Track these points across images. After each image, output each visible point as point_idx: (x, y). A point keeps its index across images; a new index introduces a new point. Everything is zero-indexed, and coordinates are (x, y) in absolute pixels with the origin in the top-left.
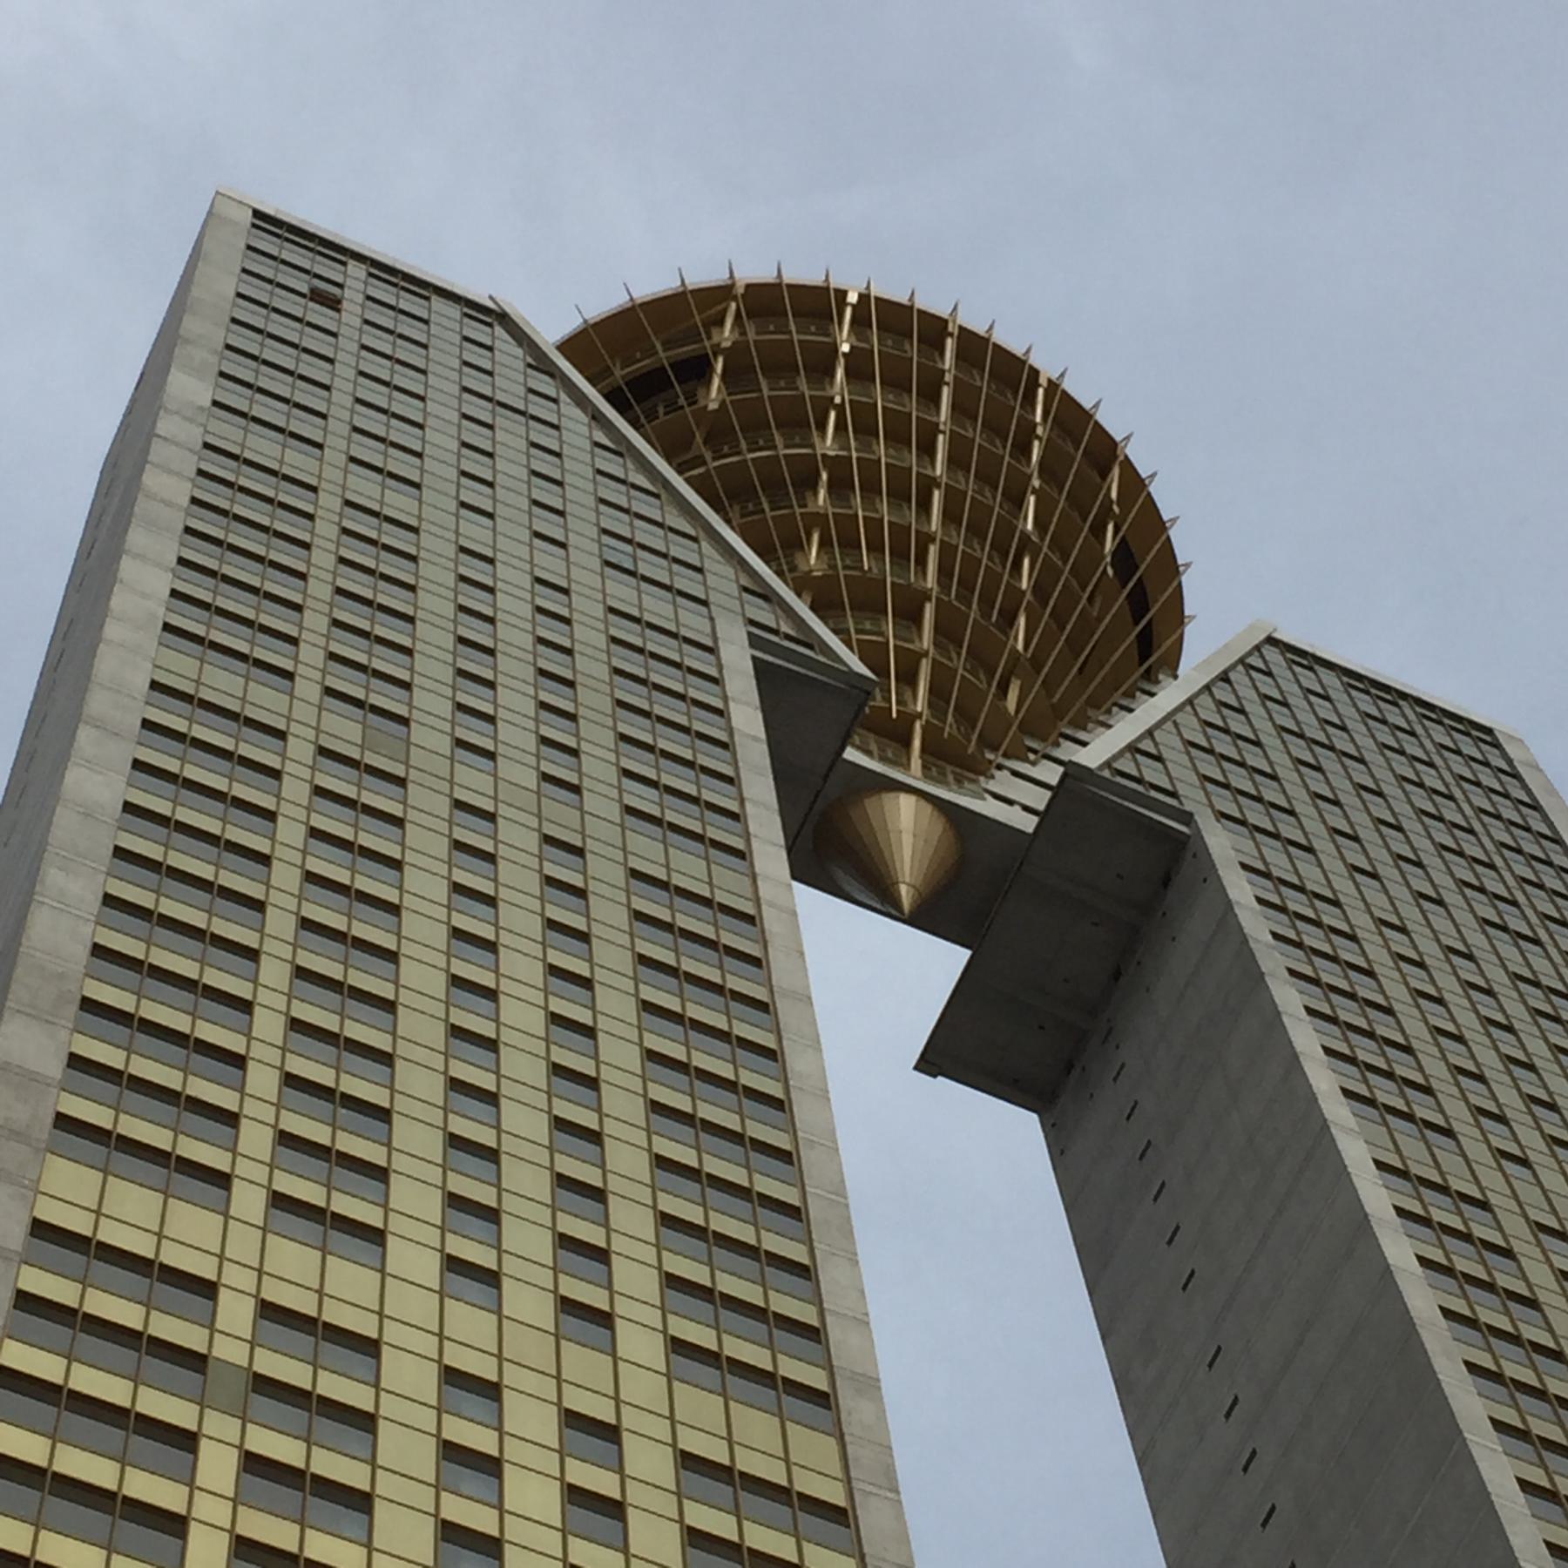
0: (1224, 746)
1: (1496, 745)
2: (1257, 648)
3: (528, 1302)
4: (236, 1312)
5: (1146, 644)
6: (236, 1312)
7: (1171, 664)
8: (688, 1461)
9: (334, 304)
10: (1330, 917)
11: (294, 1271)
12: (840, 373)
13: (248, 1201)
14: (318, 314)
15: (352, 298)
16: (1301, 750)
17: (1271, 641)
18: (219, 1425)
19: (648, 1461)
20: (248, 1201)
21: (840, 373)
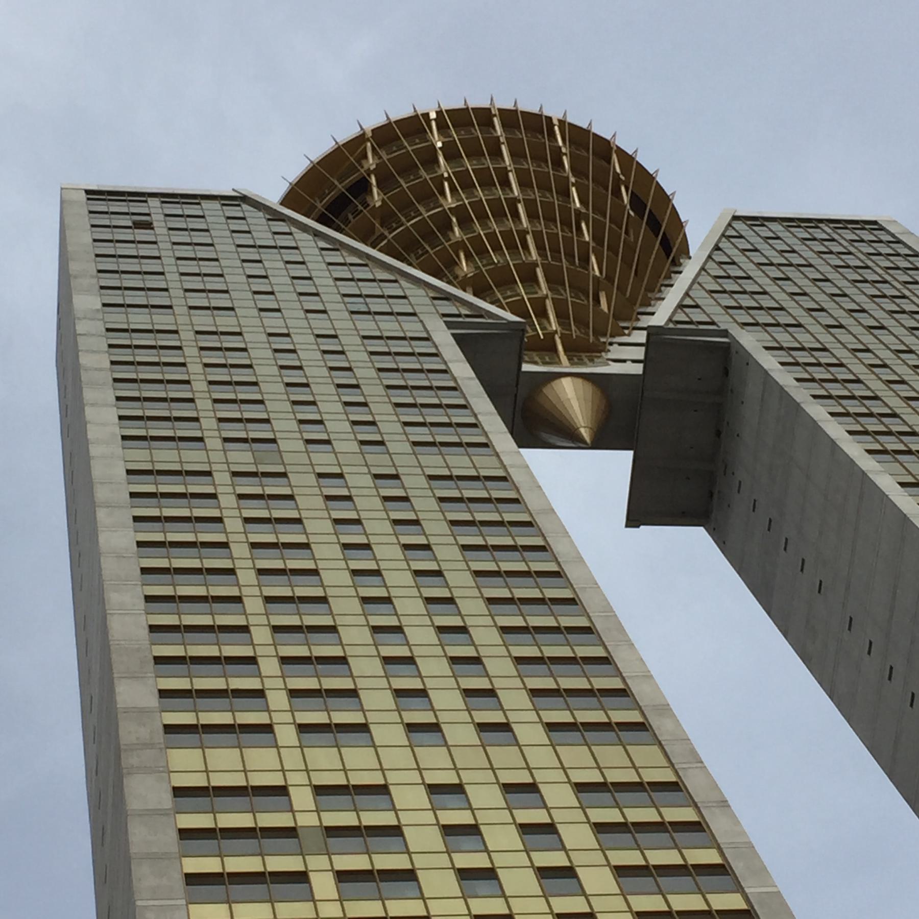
0: (730, 286)
1: (882, 229)
2: (729, 225)
3: (461, 733)
4: (302, 798)
5: (666, 246)
6: (302, 798)
7: (685, 251)
8: (581, 788)
9: (148, 226)
10: (825, 358)
11: (326, 762)
12: (441, 160)
13: (286, 735)
14: (142, 234)
15: (157, 219)
16: (775, 273)
17: (735, 218)
18: (317, 862)
19: (559, 796)
20: (286, 735)
21: (441, 160)
